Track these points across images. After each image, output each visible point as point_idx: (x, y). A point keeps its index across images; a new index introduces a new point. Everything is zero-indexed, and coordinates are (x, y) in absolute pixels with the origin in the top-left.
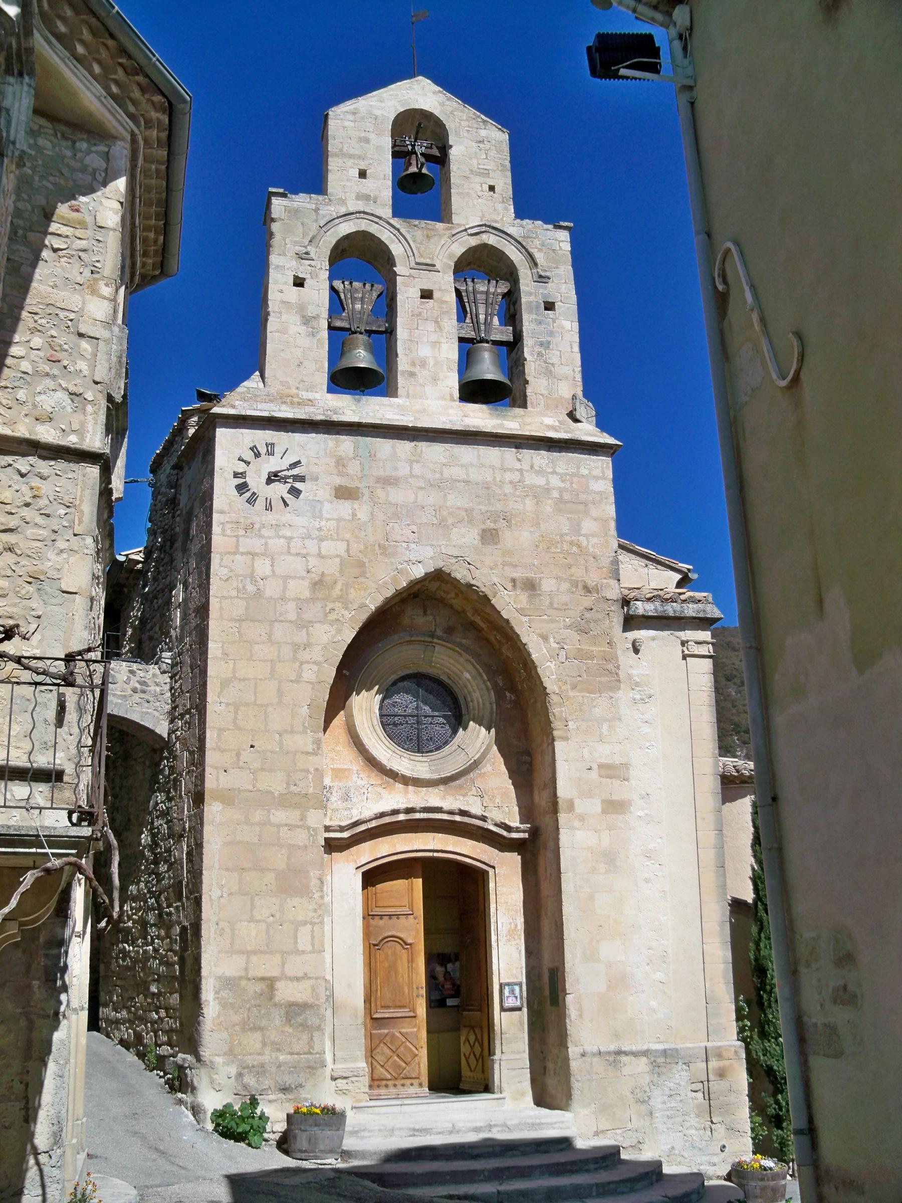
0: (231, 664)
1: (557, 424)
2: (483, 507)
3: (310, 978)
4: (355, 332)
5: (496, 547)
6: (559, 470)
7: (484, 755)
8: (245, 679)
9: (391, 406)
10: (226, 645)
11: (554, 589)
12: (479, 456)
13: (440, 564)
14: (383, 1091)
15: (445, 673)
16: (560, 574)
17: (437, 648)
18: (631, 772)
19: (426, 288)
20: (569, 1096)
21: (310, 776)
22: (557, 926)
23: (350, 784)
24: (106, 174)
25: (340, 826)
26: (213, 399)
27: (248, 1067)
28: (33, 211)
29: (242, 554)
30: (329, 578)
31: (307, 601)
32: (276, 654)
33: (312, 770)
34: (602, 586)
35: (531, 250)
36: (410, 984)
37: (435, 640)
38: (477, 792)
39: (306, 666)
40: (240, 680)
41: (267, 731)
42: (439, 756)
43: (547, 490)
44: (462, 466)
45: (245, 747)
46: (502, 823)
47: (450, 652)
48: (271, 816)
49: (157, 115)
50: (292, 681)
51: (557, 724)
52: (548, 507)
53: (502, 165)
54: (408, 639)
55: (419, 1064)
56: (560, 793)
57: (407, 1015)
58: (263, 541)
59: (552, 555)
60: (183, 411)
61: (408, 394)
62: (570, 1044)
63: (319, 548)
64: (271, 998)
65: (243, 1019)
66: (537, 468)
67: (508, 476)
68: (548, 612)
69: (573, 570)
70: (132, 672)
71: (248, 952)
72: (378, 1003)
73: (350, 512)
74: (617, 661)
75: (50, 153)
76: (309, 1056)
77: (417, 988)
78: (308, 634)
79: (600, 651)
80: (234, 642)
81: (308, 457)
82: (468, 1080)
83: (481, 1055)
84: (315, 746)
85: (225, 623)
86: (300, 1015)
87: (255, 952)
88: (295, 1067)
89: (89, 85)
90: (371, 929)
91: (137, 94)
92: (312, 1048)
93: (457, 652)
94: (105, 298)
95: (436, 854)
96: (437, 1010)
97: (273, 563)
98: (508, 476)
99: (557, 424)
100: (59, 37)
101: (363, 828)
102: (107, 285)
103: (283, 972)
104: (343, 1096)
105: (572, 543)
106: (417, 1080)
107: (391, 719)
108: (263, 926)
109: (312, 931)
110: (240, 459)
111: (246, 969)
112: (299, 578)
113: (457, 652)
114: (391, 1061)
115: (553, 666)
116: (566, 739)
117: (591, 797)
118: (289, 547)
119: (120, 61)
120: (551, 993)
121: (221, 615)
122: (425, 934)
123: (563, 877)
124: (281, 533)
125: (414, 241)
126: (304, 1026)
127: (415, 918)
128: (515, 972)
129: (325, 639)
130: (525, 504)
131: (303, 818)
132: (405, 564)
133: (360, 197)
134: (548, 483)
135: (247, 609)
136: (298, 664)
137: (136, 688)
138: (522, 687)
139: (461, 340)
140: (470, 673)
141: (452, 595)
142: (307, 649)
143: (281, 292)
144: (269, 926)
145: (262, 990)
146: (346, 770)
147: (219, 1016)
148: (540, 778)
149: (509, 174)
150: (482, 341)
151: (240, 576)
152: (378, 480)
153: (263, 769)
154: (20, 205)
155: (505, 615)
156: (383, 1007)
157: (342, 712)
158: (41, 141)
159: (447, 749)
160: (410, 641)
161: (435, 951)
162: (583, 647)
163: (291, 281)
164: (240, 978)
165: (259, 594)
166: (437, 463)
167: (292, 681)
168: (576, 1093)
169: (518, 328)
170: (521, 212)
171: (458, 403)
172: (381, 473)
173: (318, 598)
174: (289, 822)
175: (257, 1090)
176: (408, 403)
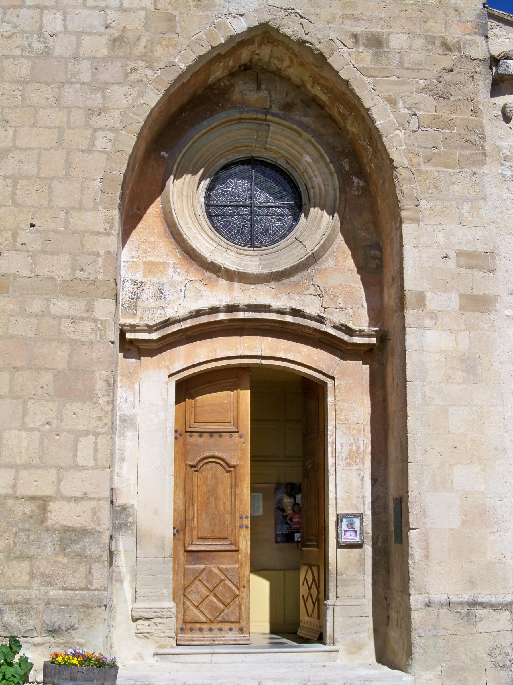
0: (11, 133)
3: (91, 499)
7: (324, 248)
11: (405, 46)
13: (266, 17)
14: (196, 636)
15: (283, 156)
16: (413, 29)
18: (498, 262)
20: (409, 654)
21: (100, 260)
22: (402, 446)
23: (165, 279)
25: (147, 326)
27: (10, 603)
29: (29, 8)
30: (131, 33)
31: (104, 59)
32: (65, 119)
33: (102, 252)
34: (465, 43)
36: (232, 513)
37: (269, 117)
38: (316, 290)
40: (21, 149)
41: (51, 207)
45: (23, 226)
46: (342, 325)
47: (288, 132)
48: (51, 306)
50: (83, 151)
51: (405, 203)
54: (237, 116)
55: (240, 606)
56: (406, 286)
57: (228, 548)
62: (412, 591)
65: (9, 544)
68: (398, 72)
69: (429, 24)
71: (17, 466)
72: (194, 533)
74: (483, 131)
76: (86, 592)
77: (241, 518)
78: (104, 97)
79: (462, 120)
80: (16, 107)
82: (306, 626)
83: (318, 598)
84: (107, 226)
85: (6, 85)
86: (76, 542)
87: (25, 467)
88: (68, 605)
92: (90, 582)
93: (295, 130)
95: (264, 362)
96: (286, 545)
97: (65, 17)
101: (175, 328)
103: (58, 490)
104: (145, 640)
106: (237, 625)
107: (220, 210)
108: (36, 435)
109: (96, 443)
111: (14, 486)
113: (295, 130)
114: (206, 602)
115: (401, 135)
116: (417, 221)
117: (446, 291)
120: (395, 530)
123: (409, 386)
126: (81, 556)
128: (355, 502)
129: (124, 103)
131: (89, 309)
132: (224, 18)
135: (33, 69)
136: (90, 132)
138: (370, 167)
140: (311, 156)
141: (287, 62)
142: (103, 114)
144: (43, 435)
145: (32, 511)
146: (161, 263)
148: (389, 274)
151: (26, 32)
153: (44, 252)
155: (344, 75)
156: (199, 538)
157: (159, 199)
159: (283, 243)
160: (240, 119)
161: (283, 481)
162: (440, 114)
164: (7, 497)
165: (47, 52)
167: (83, 151)
168: (417, 651)
173: (117, 57)
174: (72, 313)
175: (19, 630)
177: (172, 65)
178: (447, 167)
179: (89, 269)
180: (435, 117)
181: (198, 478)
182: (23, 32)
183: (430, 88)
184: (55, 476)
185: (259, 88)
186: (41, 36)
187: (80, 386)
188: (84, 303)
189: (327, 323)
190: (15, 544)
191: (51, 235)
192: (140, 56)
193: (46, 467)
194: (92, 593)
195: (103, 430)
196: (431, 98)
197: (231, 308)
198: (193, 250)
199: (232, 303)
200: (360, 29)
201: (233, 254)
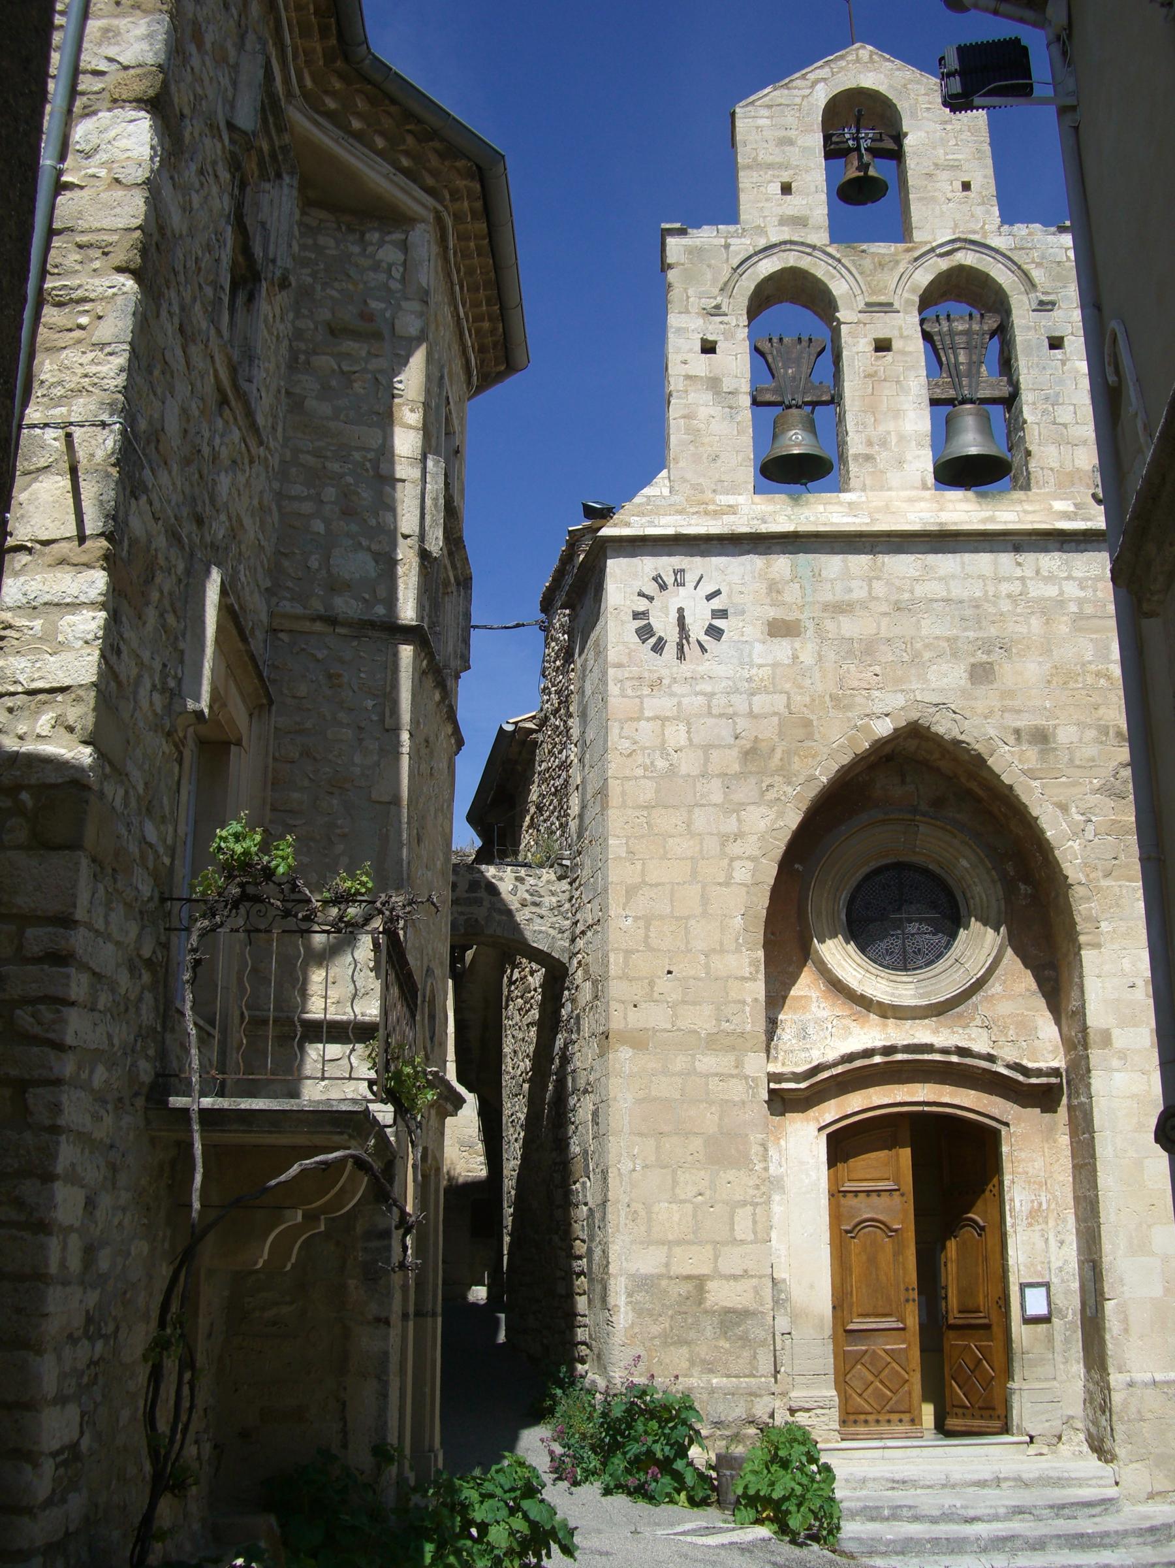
1: (1072, 508)
2: (971, 634)
4: (789, 407)
5: (991, 687)
6: (1076, 574)
8: (657, 885)
9: (840, 503)
10: (632, 840)
11: (1074, 740)
12: (963, 563)
13: (914, 715)
16: (1082, 718)
17: (922, 828)
19: (881, 336)
21: (748, 1009)
24: (405, 269)
26: (605, 514)
28: (316, 328)
29: (648, 719)
30: (764, 744)
32: (697, 849)
33: (749, 1000)
35: (1025, 267)
37: (918, 817)
39: (737, 864)
42: (937, 971)
43: (1061, 603)
44: (941, 579)
45: (660, 973)
48: (697, 1063)
49: (464, 182)
50: (719, 884)
52: (1063, 628)
53: (978, 151)
56: (1089, 1023)
57: (894, 1325)
58: (675, 701)
59: (1071, 693)
60: (570, 532)
61: (864, 485)
63: (750, 705)
64: (700, 1302)
66: (1046, 574)
67: (1005, 588)
69: (1101, 711)
70: (520, 880)
71: (669, 1242)
72: (855, 1309)
73: (790, 653)
75: (334, 252)
78: (739, 820)
80: (643, 836)
81: (729, 584)
84: (752, 969)
85: (629, 812)
86: (738, 1325)
87: (679, 1243)
88: (733, 1394)
89: (371, 163)
90: (842, 1209)
91: (435, 162)
94: (410, 427)
95: (926, 1109)
98: (1005, 588)
99: (1072, 508)
100: (329, 115)
102: (412, 410)
105: (1098, 674)
108: (689, 1206)
109: (754, 1214)
110: (641, 594)
111: (667, 1265)
112: (724, 747)
116: (1098, 946)
117: (1135, 1026)
118: (709, 707)
119: (408, 127)
121: (624, 802)
122: (915, 1215)
124: (698, 688)
125: (861, 273)
126: (745, 1340)
127: (902, 1195)
128: (1039, 1268)
129: (762, 825)
130: (1029, 625)
131: (739, 1064)
133: (784, 221)
134: (1061, 593)
135: (657, 791)
136: (726, 861)
137: (525, 900)
139: (934, 402)
142: (739, 841)
143: (685, 363)
144: (696, 1207)
145: (689, 1292)
146: (802, 997)
147: (632, 1326)
149: (989, 162)
150: (964, 401)
151: (646, 748)
152: (826, 607)
153: (684, 1002)
154: (300, 324)
155: (1006, 779)
158: (322, 240)
159: (941, 965)
163: (698, 347)
164: (660, 1276)
165: (672, 771)
166: (904, 578)
169: (1015, 378)
170: (1009, 216)
171: (933, 492)
172: (828, 597)
173: (750, 773)
174: (720, 1070)
176: (864, 499)
177: (811, 779)
178: (1130, 881)
179: (736, 1020)
180: (1114, 822)
181: (855, 1245)
182: (644, 748)
183: (1106, 788)
184: (712, 1252)
185: (903, 782)
186: (664, 754)
187: (733, 1151)
188: (733, 1058)
189: (1000, 1062)
190: (672, 1329)
191: (692, 982)
192: (776, 771)
193: (700, 1243)
194: (758, 1380)
195: (762, 1200)
196: (1108, 799)
197: (888, 1050)
198: (840, 981)
199: (888, 1044)
200: (1024, 722)
201: (884, 982)
